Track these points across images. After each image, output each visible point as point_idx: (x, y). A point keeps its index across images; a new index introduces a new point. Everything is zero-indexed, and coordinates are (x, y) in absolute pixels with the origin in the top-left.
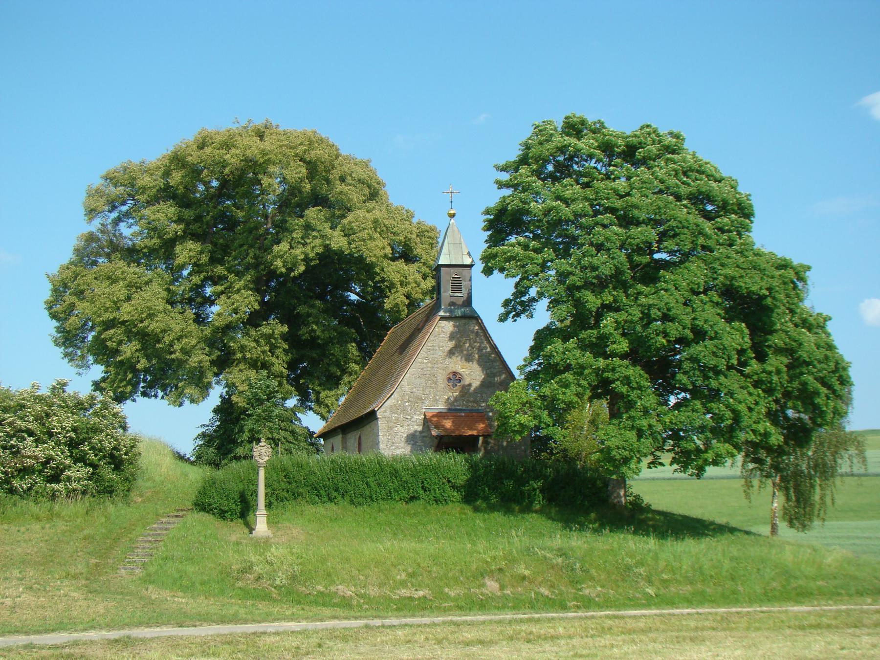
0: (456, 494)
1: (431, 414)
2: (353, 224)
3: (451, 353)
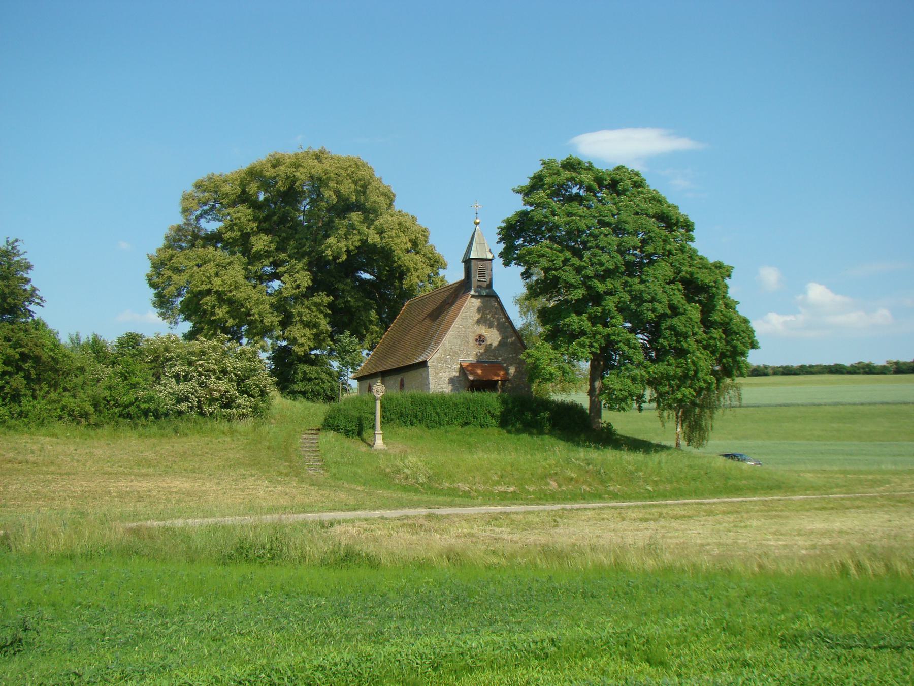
3: (478, 322)
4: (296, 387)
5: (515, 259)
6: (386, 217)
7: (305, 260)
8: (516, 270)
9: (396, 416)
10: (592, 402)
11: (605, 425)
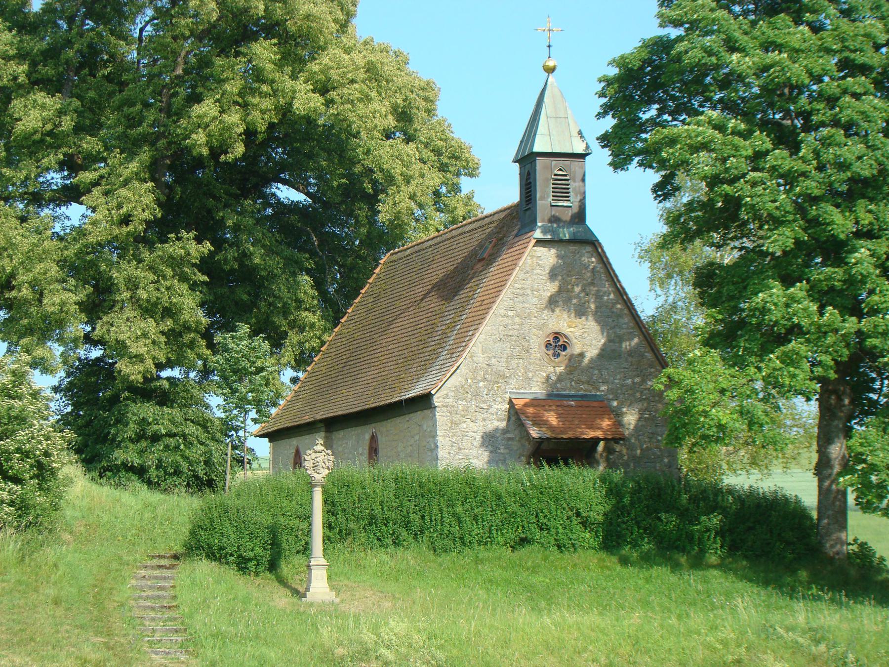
0: (588, 535)
1: (522, 402)
2: (332, 72)
3: (552, 303)
4: (119, 456)
5: (638, 153)
6: (334, 51)
7: (145, 155)
8: (642, 179)
9: (360, 523)
10: (823, 493)
11: (855, 548)
